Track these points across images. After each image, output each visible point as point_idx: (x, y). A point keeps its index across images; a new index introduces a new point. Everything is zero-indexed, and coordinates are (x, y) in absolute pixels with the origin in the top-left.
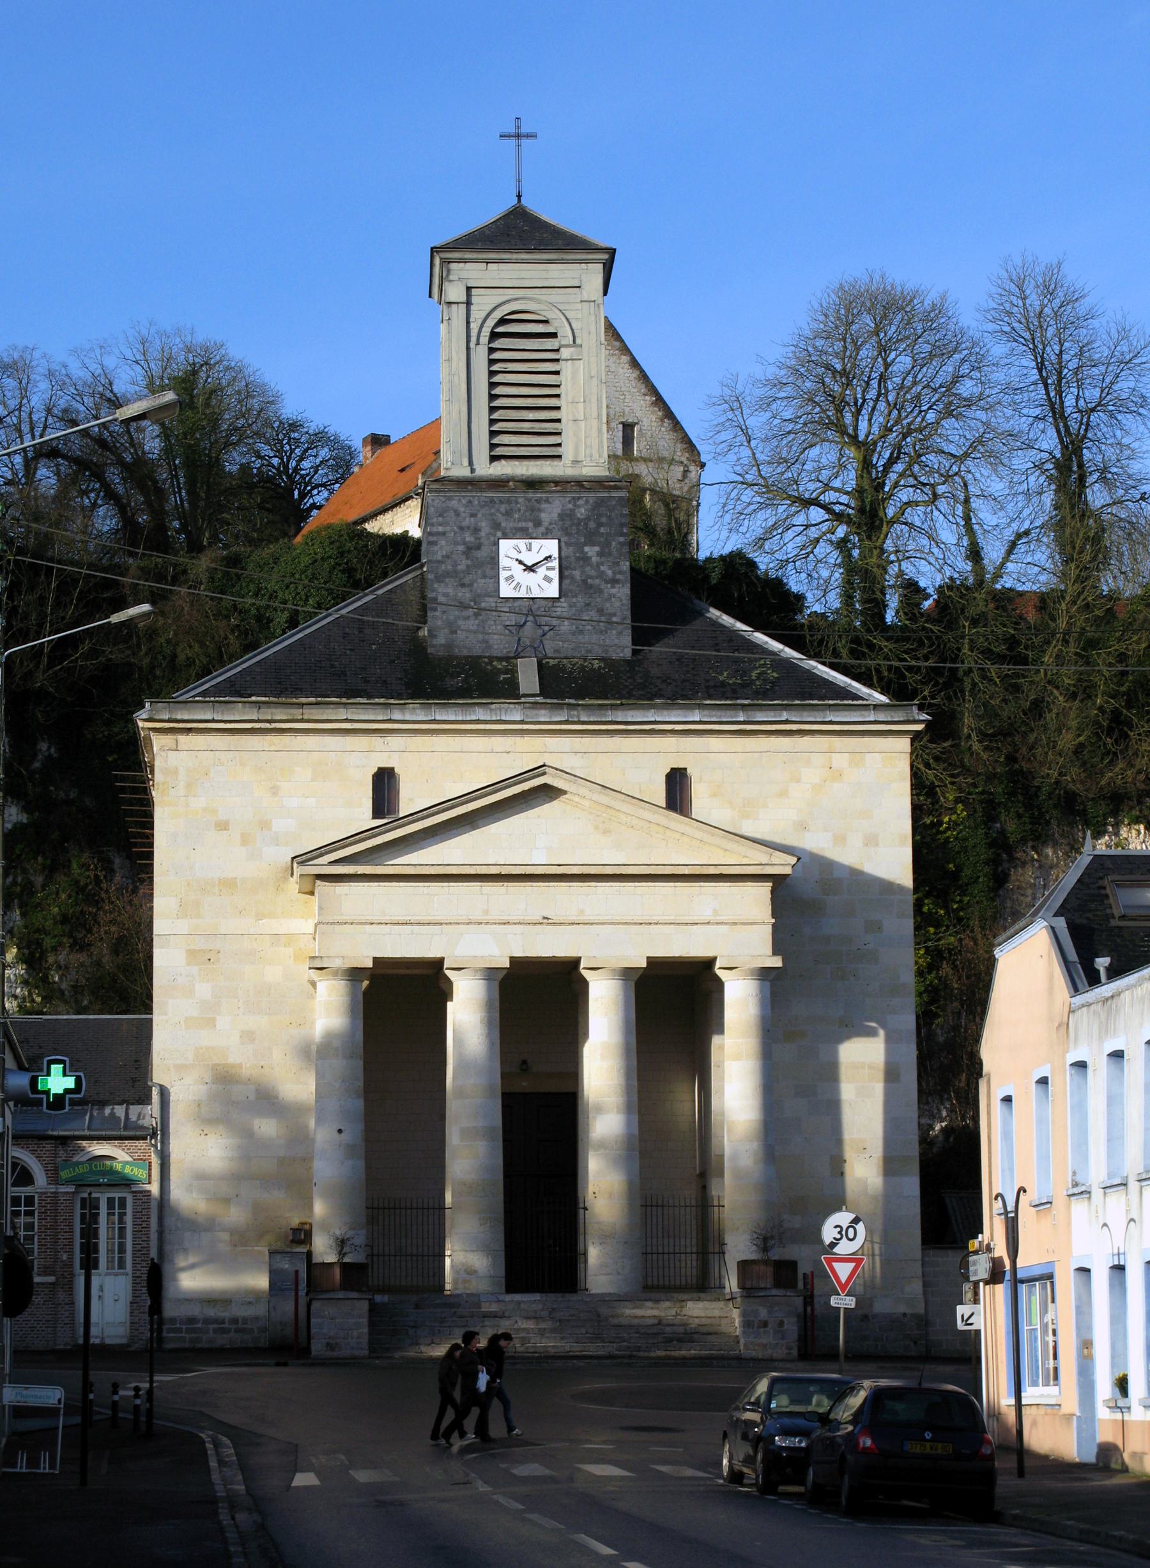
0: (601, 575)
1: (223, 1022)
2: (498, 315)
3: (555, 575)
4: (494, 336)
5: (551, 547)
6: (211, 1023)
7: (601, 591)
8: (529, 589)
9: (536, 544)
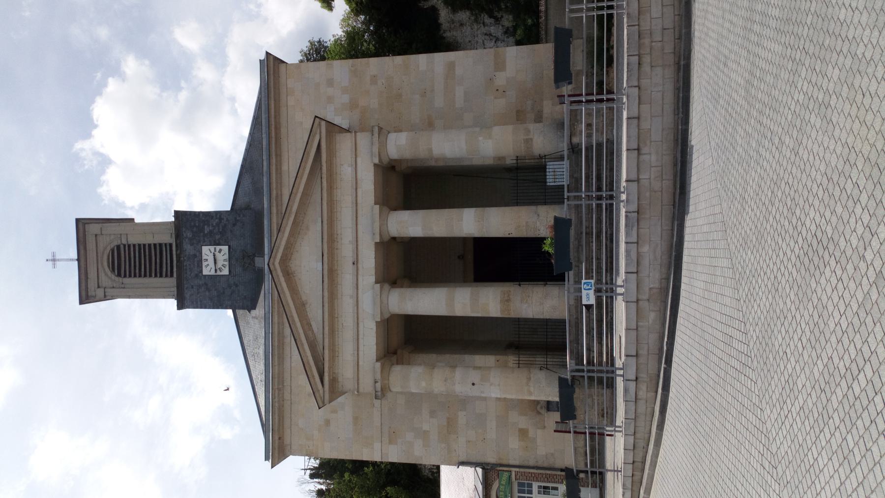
0: (218, 225)
1: (426, 427)
2: (109, 273)
3: (218, 248)
4: (119, 275)
5: (205, 249)
6: (426, 432)
7: (225, 225)
8: (225, 260)
9: (204, 257)
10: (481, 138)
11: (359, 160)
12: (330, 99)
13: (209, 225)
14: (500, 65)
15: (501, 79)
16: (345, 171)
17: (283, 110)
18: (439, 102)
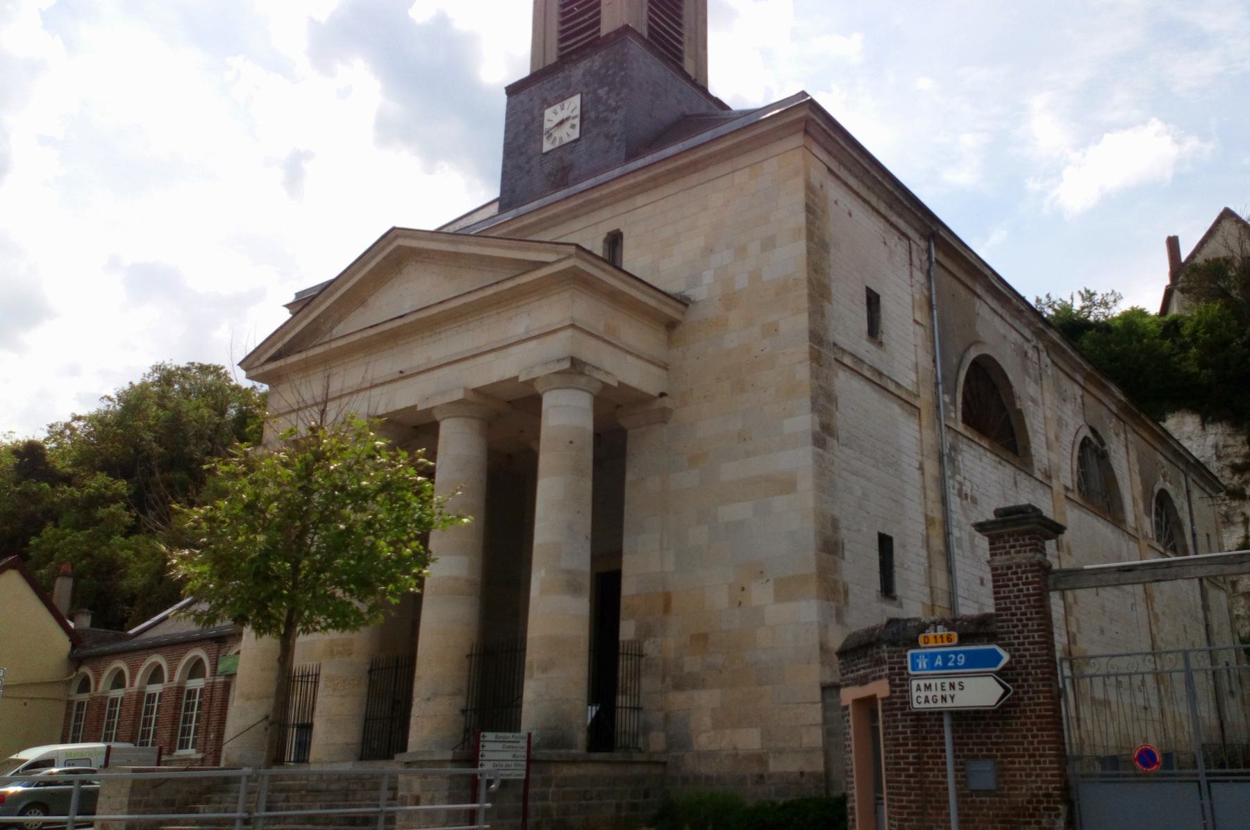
9: (566, 103)
10: (33, 541)
11: (532, 345)
12: (741, 251)
13: (608, 93)
14: (786, 590)
15: (761, 594)
16: (520, 323)
17: (725, 167)
18: (730, 471)
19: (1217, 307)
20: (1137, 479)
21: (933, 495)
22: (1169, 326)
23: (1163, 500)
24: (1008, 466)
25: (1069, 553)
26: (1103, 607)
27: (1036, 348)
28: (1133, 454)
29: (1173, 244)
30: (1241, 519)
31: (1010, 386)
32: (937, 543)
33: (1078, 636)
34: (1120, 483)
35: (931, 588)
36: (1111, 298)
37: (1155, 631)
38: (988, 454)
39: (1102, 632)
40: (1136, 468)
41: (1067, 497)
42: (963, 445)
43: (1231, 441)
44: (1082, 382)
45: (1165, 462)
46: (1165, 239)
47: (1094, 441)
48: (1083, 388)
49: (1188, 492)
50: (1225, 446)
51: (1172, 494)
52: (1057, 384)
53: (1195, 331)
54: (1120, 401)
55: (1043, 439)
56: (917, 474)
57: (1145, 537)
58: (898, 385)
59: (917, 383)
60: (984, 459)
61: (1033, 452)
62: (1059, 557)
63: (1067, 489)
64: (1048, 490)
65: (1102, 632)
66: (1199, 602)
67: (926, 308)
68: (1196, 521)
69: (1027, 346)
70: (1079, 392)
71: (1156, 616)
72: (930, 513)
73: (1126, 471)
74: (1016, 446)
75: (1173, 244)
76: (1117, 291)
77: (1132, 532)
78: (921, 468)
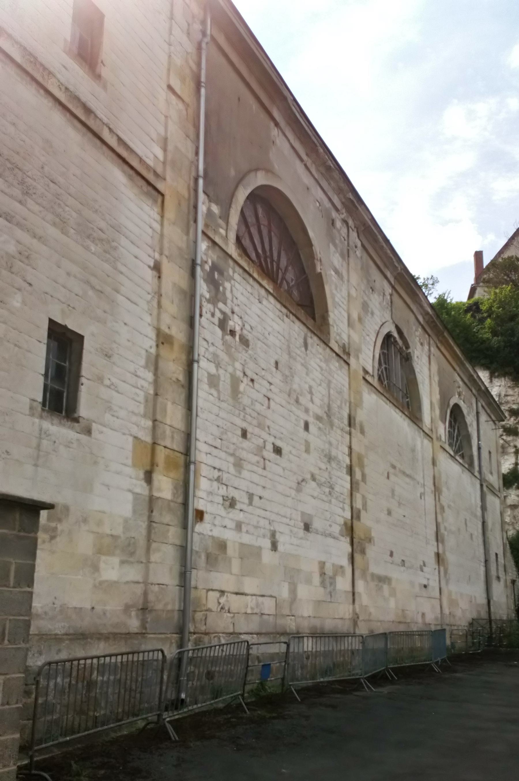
19: (509, 288)
20: (436, 389)
21: (173, 307)
22: (474, 307)
23: (456, 416)
24: (298, 323)
25: (362, 432)
26: (393, 491)
27: (345, 222)
28: (435, 368)
29: (478, 256)
30: (513, 450)
31: (310, 244)
32: (174, 369)
33: (363, 514)
34: (421, 387)
35: (155, 421)
36: (431, 282)
37: (440, 519)
38: (271, 299)
39: (389, 513)
40: (436, 379)
41: (364, 378)
42: (231, 270)
43: (510, 392)
44: (392, 280)
45: (461, 383)
46: (473, 253)
47: (396, 334)
48: (393, 287)
49: (478, 413)
50: (506, 395)
51: (465, 411)
52: (365, 270)
53: (491, 307)
54: (427, 313)
55: (346, 315)
56: (149, 275)
57: (439, 439)
58: (141, 160)
59: (164, 163)
60: (265, 302)
61: (331, 322)
62: (350, 434)
63: (366, 372)
64: (346, 367)
65: (389, 513)
66: (479, 503)
67: (192, 85)
68: (482, 438)
69: (334, 214)
70: (388, 290)
71: (442, 508)
72: (164, 328)
73: (427, 381)
74: (314, 314)
75: (478, 256)
76: (435, 276)
77: (427, 431)
78: (157, 268)
